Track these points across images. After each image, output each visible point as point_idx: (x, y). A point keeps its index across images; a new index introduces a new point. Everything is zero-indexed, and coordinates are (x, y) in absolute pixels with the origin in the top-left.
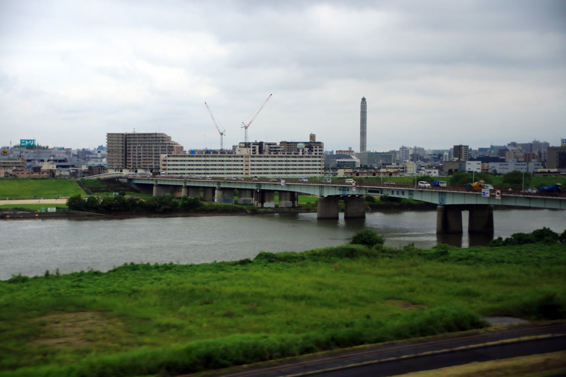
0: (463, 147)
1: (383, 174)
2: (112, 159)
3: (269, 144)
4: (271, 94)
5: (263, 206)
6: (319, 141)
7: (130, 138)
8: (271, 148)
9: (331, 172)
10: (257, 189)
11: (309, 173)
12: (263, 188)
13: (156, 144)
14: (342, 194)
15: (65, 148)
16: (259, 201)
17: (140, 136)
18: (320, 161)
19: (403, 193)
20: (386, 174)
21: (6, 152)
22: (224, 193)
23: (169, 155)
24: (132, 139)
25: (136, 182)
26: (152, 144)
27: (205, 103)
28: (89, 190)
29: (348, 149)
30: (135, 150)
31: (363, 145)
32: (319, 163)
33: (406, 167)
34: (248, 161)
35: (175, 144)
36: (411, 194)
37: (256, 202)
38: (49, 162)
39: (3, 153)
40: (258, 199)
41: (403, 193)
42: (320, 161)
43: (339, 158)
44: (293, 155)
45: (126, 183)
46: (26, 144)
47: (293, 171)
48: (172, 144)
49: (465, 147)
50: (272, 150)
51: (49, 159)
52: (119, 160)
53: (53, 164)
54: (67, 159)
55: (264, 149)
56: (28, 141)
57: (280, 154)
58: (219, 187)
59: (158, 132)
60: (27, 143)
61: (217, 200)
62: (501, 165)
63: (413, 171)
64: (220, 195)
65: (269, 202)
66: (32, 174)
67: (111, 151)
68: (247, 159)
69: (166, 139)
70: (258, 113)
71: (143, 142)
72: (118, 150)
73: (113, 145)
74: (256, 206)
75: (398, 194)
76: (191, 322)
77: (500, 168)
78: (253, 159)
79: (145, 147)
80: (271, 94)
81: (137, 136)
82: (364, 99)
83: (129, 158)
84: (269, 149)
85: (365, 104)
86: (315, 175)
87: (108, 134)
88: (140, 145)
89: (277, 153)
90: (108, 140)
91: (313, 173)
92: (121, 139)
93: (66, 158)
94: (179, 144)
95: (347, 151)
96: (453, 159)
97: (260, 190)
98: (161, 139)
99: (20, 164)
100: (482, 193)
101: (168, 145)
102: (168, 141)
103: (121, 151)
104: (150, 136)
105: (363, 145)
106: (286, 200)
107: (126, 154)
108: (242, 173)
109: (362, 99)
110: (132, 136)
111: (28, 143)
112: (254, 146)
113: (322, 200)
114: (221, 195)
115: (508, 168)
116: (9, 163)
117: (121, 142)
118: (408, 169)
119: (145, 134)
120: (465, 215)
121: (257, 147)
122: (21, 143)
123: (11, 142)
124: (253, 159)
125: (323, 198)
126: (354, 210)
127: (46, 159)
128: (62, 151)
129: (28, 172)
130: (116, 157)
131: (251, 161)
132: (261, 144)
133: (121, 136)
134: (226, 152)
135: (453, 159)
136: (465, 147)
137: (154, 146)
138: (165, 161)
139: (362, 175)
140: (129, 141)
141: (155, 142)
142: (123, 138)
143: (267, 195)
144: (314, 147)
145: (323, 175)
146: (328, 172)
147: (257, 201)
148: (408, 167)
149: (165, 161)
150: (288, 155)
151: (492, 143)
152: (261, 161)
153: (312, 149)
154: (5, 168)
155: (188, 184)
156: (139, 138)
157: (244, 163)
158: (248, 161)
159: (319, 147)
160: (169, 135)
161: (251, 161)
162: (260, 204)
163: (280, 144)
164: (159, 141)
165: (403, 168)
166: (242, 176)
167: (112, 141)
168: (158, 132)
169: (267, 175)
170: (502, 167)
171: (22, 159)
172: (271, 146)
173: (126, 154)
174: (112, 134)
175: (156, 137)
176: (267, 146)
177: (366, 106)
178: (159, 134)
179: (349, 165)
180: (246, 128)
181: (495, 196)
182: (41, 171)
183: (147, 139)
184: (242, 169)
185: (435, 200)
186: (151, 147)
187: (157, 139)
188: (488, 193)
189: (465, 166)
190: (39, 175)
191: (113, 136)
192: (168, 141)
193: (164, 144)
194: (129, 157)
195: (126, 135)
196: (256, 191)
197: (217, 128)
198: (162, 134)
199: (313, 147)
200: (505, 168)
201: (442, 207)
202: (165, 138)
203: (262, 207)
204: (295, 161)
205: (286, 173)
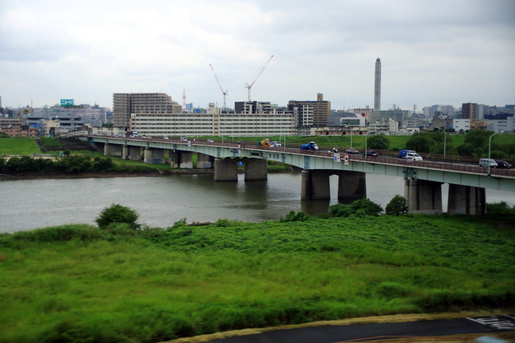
0: (471, 105)
1: (354, 132)
2: (118, 118)
3: (263, 103)
4: (272, 56)
5: (180, 167)
6: (326, 100)
7: (134, 98)
8: (264, 107)
9: (305, 130)
10: (174, 149)
11: (272, 132)
12: (178, 149)
13: (157, 103)
14: (233, 156)
15: (100, 106)
16: (175, 161)
17: (143, 96)
18: (290, 120)
20: (357, 133)
21: (28, 111)
22: (153, 153)
23: (137, 114)
24: (136, 99)
25: (95, 140)
26: (153, 103)
27: (210, 65)
28: (45, 148)
29: (365, 108)
30: (138, 109)
31: (377, 103)
32: (290, 122)
33: (388, 126)
34: (217, 120)
35: (174, 104)
36: (284, 158)
37: (172, 162)
38: (55, 120)
39: (24, 112)
40: (174, 159)
42: (290, 120)
43: (344, 117)
44: (284, 114)
45: (86, 141)
46: (66, 104)
47: (263, 130)
48: (171, 104)
49: (473, 105)
50: (265, 109)
51: (54, 117)
52: (124, 118)
53: (58, 122)
54: (81, 118)
55: (257, 108)
56: (67, 100)
57: (244, 113)
58: (148, 147)
59: (159, 92)
60: (66, 102)
61: (146, 160)
62: (500, 122)
63: (396, 130)
64: (149, 155)
65: (187, 163)
66: (21, 131)
67: (117, 110)
68: (216, 118)
69: (167, 98)
70: (260, 74)
71: (145, 102)
72: (124, 109)
73: (119, 105)
74: (172, 167)
76: (395, 250)
77: (498, 126)
78: (222, 118)
79: (148, 106)
80: (272, 56)
81: (141, 96)
82: (378, 60)
84: (263, 108)
85: (379, 64)
86: (279, 134)
87: (115, 94)
88: (143, 105)
89: (268, 113)
90: (114, 100)
91: (276, 132)
92: (126, 99)
93: (80, 117)
94: (178, 103)
95: (364, 110)
96: (442, 117)
98: (161, 99)
99: (19, 122)
100: (334, 158)
101: (167, 105)
102: (168, 100)
103: (126, 110)
104: (152, 96)
105: (377, 103)
106: (204, 160)
108: (211, 132)
109: (377, 60)
110: (136, 96)
111: (67, 102)
112: (247, 105)
113: (219, 162)
114: (150, 155)
115: (506, 126)
116: (8, 121)
117: (126, 102)
118: (391, 128)
119: (147, 94)
120: (334, 181)
121: (251, 106)
122: (62, 102)
123: (32, 102)
124: (222, 118)
125: (220, 159)
126: (255, 172)
127: (51, 118)
128: (97, 110)
129: (17, 130)
130: (122, 116)
131: (221, 120)
132: (254, 104)
133: (126, 96)
134: (228, 112)
135: (442, 117)
136: (473, 105)
137: (155, 105)
138: (134, 120)
139: (332, 133)
140: (134, 101)
141: (156, 102)
142: (127, 98)
143: (183, 156)
144: (304, 106)
145: (297, 134)
146: (302, 130)
147: (173, 161)
148: (390, 125)
149: (134, 120)
150: (286, 114)
151: (20, 105)
152: (265, 120)
153: (302, 108)
155: (128, 144)
156: (142, 98)
157: (213, 122)
158: (217, 120)
159: (309, 106)
160: (169, 95)
161: (221, 120)
162: (177, 164)
163: (289, 103)
164: (160, 100)
165: (386, 126)
166: (211, 134)
167: (118, 100)
168: (159, 92)
169: (230, 134)
170: (500, 124)
171: (21, 117)
172: (265, 105)
174: (118, 94)
175: (157, 97)
176: (261, 106)
177: (381, 67)
178: (160, 94)
179: (353, 123)
180: (249, 88)
182: (30, 129)
183: (149, 99)
184: (211, 128)
185: (301, 164)
186: (153, 106)
187: (158, 99)
188: (338, 158)
189: (452, 124)
190: (28, 133)
191: (119, 96)
192: (168, 100)
193: (164, 103)
195: (131, 95)
196: (173, 151)
197: (221, 88)
198: (162, 94)
199: (302, 106)
200: (504, 126)
201: (306, 171)
202: (165, 98)
203: (179, 168)
204: (265, 120)
205: (255, 132)
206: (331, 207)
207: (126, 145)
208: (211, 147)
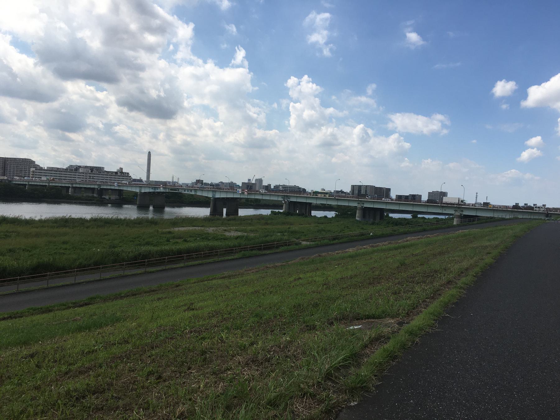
7: (7, 160)
10: (98, 188)
19: (191, 191)
25: (14, 182)
41: (191, 191)
68: (86, 175)
75: (188, 192)
82: (149, 153)
83: (7, 174)
97: (100, 188)
98: (29, 162)
107: (5, 170)
154: (63, 303)
173: (5, 170)
181: (244, 193)
194: (6, 173)
206: (428, 201)
207: (72, 186)
208: (217, 191)
